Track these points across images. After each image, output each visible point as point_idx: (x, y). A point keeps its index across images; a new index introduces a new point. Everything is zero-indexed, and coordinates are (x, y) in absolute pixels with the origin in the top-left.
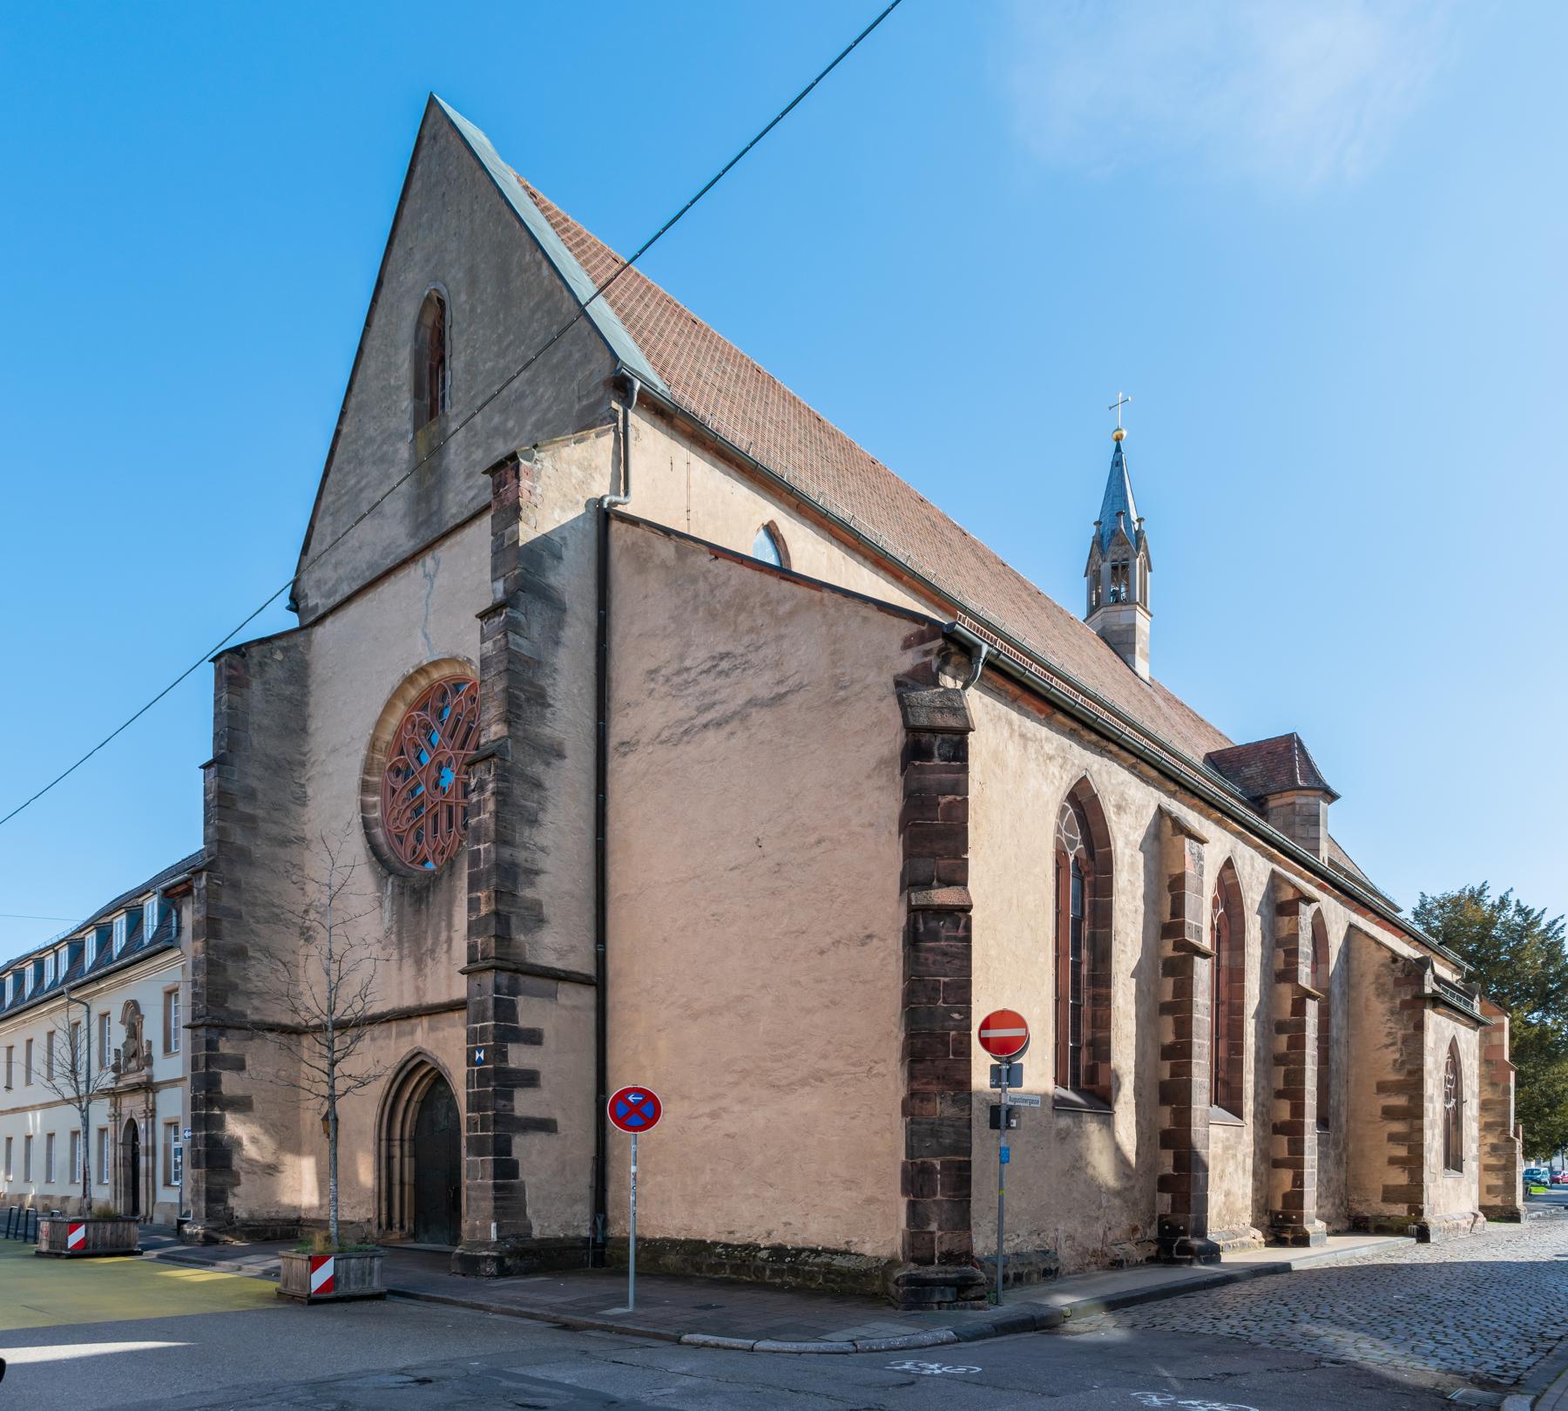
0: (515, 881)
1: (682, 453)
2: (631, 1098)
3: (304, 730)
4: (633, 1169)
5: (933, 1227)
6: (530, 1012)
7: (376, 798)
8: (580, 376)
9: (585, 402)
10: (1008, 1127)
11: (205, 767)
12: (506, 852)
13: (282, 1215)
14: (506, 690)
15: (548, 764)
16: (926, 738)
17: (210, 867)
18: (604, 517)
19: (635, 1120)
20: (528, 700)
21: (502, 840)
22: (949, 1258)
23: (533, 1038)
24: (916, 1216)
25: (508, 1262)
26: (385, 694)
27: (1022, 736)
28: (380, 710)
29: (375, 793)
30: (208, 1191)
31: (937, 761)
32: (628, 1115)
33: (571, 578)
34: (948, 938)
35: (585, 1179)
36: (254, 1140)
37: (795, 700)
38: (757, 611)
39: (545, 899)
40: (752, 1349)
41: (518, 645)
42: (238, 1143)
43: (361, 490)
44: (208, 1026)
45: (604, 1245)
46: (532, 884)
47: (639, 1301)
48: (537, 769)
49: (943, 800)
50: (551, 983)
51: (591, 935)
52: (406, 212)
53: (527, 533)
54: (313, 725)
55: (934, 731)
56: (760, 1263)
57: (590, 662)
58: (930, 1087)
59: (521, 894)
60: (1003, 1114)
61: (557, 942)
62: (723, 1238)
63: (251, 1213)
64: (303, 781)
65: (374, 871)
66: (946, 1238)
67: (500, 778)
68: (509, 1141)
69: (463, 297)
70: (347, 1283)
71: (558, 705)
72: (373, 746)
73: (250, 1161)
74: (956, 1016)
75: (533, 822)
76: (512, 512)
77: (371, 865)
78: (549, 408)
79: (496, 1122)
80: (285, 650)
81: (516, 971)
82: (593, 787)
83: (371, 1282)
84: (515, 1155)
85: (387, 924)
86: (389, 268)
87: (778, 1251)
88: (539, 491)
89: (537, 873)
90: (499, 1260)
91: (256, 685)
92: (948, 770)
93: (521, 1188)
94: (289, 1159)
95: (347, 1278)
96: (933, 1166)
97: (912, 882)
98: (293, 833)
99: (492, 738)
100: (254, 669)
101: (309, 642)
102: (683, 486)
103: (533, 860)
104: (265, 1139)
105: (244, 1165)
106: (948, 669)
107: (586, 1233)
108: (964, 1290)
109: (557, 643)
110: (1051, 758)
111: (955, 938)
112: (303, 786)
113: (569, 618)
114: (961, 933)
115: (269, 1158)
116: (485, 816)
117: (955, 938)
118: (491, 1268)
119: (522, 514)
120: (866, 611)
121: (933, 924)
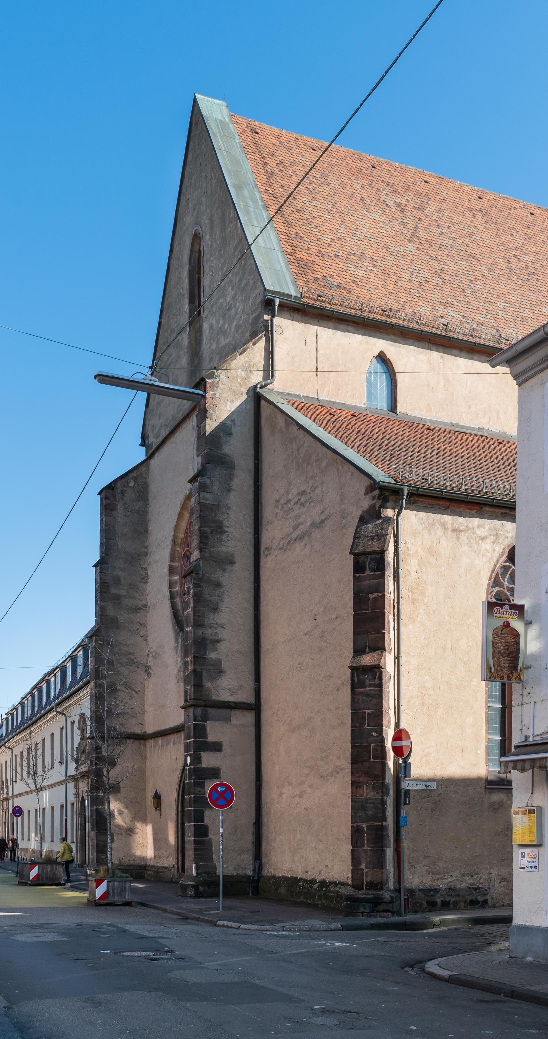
0: (205, 649)
1: (312, 330)
2: (219, 789)
3: (146, 531)
4: (221, 830)
5: (363, 866)
6: (214, 731)
7: (177, 577)
8: (252, 297)
9: (254, 315)
10: (405, 803)
11: (95, 566)
12: (200, 632)
13: (137, 862)
14: (199, 529)
15: (224, 570)
16: (362, 558)
17: (201, 558)
18: (257, 398)
19: (221, 802)
20: (212, 532)
21: (198, 624)
22: (372, 886)
23: (217, 747)
24: (356, 861)
25: (201, 889)
26: (177, 509)
27: (455, 530)
28: (176, 518)
29: (177, 574)
30: (97, 845)
31: (368, 573)
32: (218, 799)
33: (238, 448)
34: (370, 685)
35: (250, 837)
36: (120, 812)
37: (328, 524)
38: (314, 464)
39: (223, 658)
40: (239, 928)
41: (206, 499)
42: (111, 815)
43: (169, 365)
44: (194, 706)
45: (258, 881)
46: (215, 649)
47: (224, 908)
48: (218, 575)
49: (372, 597)
50: (226, 711)
51: (252, 677)
52: (186, 174)
53: (210, 425)
54: (151, 526)
55: (366, 554)
56: (314, 891)
57: (251, 496)
58: (361, 779)
59: (208, 656)
60: (403, 794)
61: (229, 686)
62: (304, 876)
63: (120, 860)
64: (146, 566)
65: (175, 630)
66: (370, 873)
67: (196, 586)
68: (202, 814)
69: (208, 237)
70: (113, 896)
71: (230, 530)
72: (174, 543)
73: (119, 826)
74: (374, 734)
75: (216, 609)
76: (204, 415)
77: (173, 625)
78: (241, 318)
79: (195, 802)
80: (135, 479)
81: (205, 706)
82: (252, 579)
83: (125, 896)
84: (206, 822)
85: (179, 666)
86: (179, 212)
87: (323, 883)
88: (217, 396)
89: (218, 642)
90: (196, 887)
91: (120, 507)
92: (374, 577)
93: (210, 843)
94: (139, 825)
95: (113, 892)
96: (363, 828)
97: (358, 651)
98: (141, 603)
99: (195, 559)
100: (118, 496)
101: (148, 469)
102: (314, 353)
103: (216, 633)
104: (125, 811)
105: (116, 829)
106: (388, 504)
107: (250, 873)
108: (376, 904)
109: (229, 490)
110: (483, 539)
111: (374, 685)
112: (146, 569)
113: (237, 472)
114: (377, 682)
115: (129, 824)
116: (190, 610)
117: (374, 685)
118: (191, 892)
119: (208, 415)
120: (352, 469)
121: (362, 677)
